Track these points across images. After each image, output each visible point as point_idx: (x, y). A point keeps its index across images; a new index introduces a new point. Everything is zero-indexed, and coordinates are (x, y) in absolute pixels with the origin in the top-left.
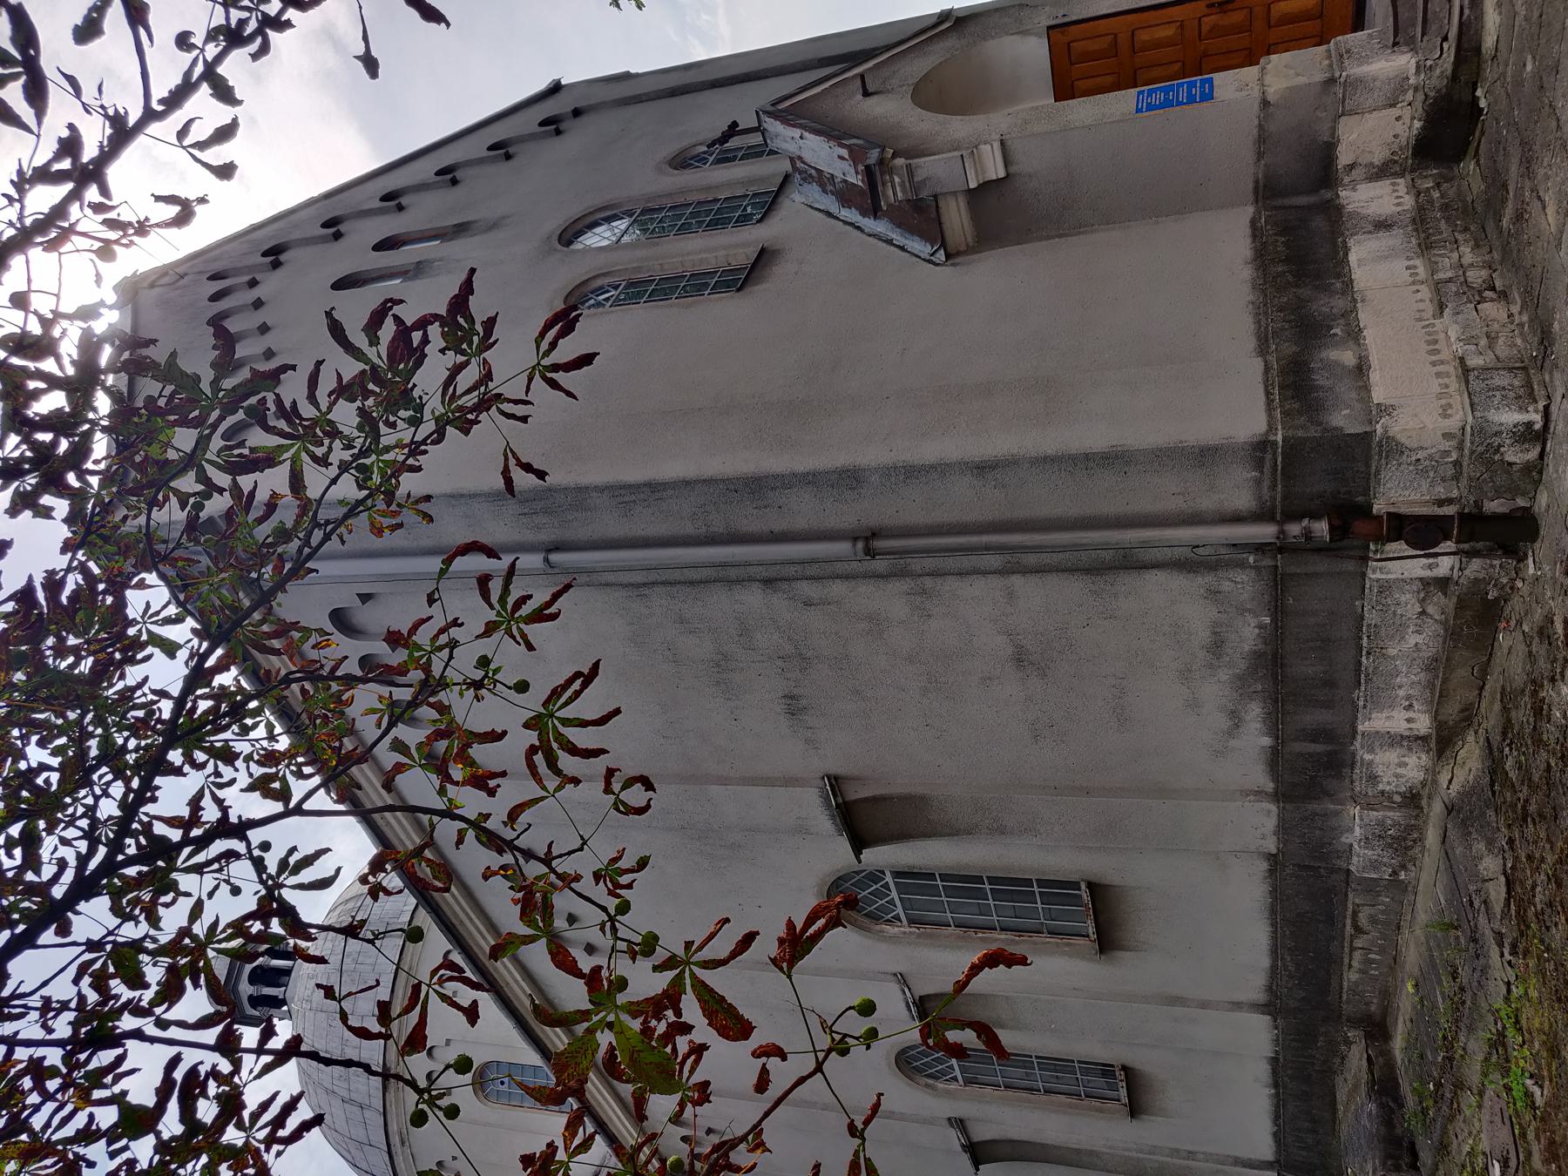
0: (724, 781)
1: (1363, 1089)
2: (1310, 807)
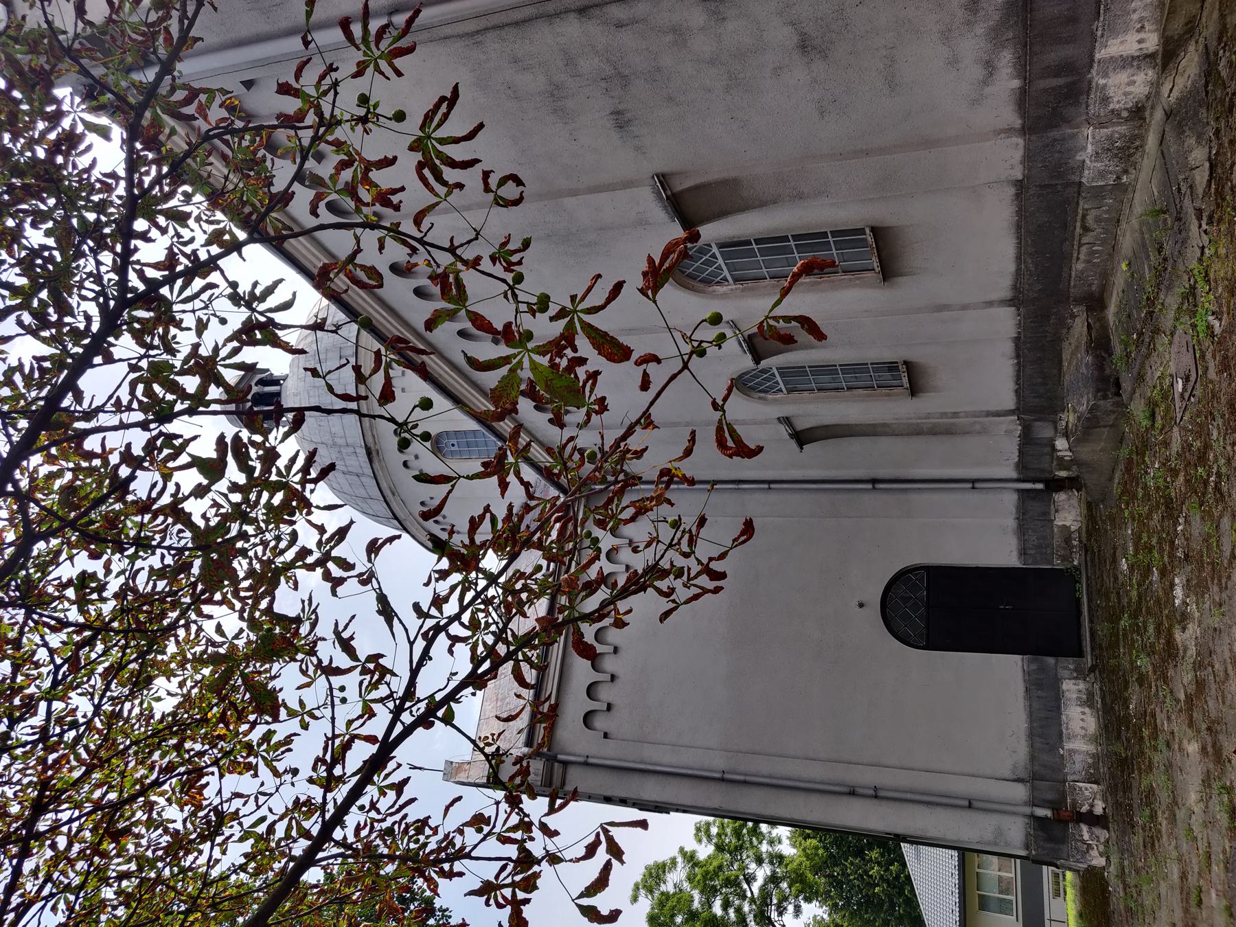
0: (574, 193)
1: (1083, 347)
2: (1051, 134)
